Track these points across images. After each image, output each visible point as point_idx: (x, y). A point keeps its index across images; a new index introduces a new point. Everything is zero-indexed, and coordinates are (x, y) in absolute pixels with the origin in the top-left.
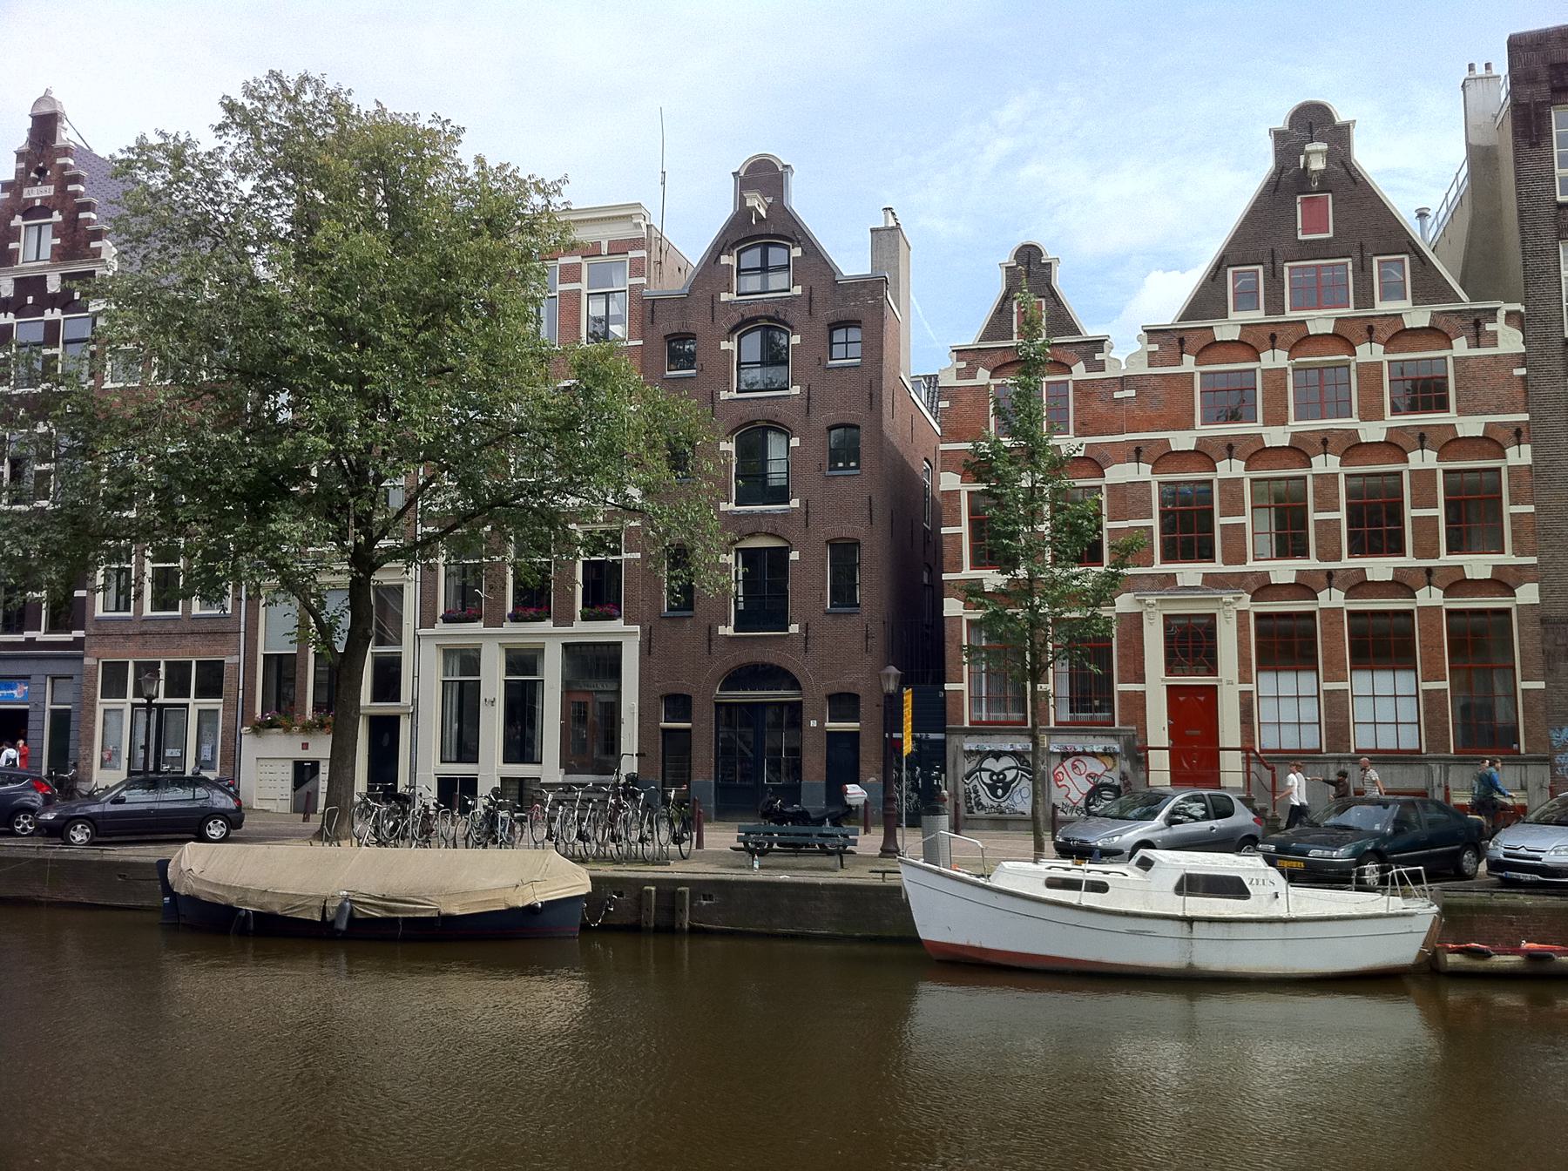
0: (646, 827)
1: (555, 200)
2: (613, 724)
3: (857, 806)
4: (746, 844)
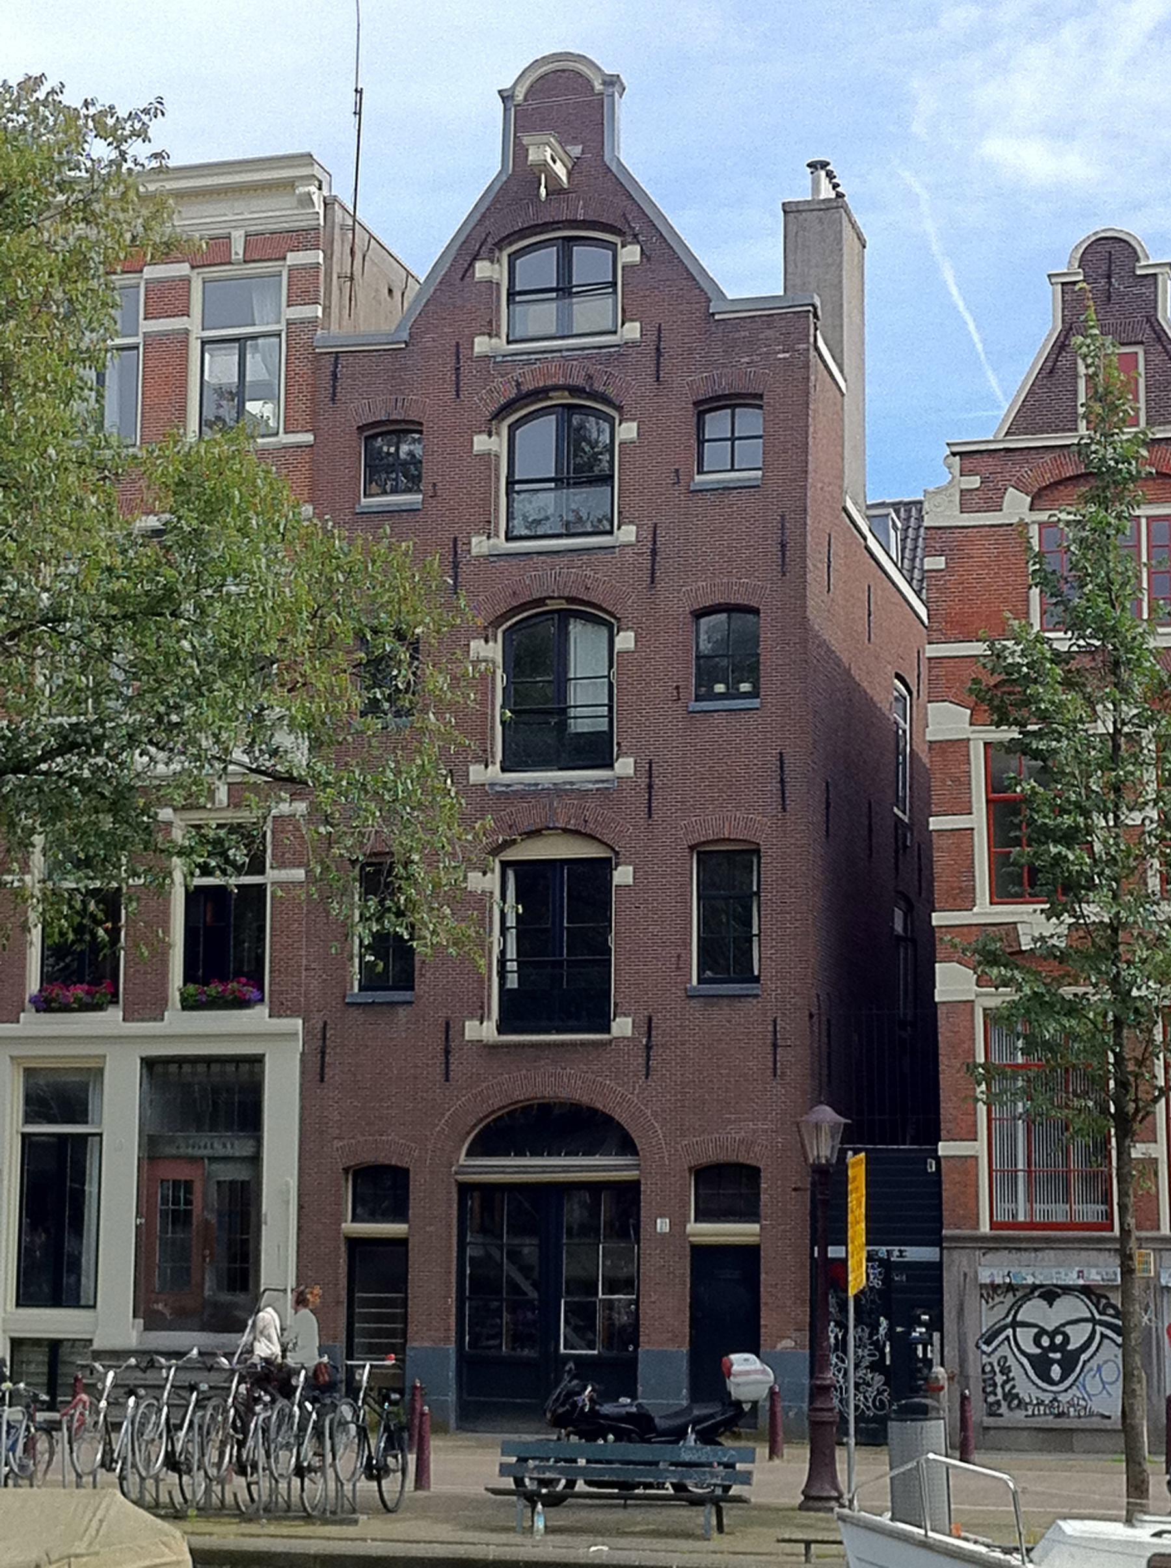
0: (308, 1446)
1: (137, 149)
2: (245, 1229)
3: (755, 1403)
4: (519, 1482)
